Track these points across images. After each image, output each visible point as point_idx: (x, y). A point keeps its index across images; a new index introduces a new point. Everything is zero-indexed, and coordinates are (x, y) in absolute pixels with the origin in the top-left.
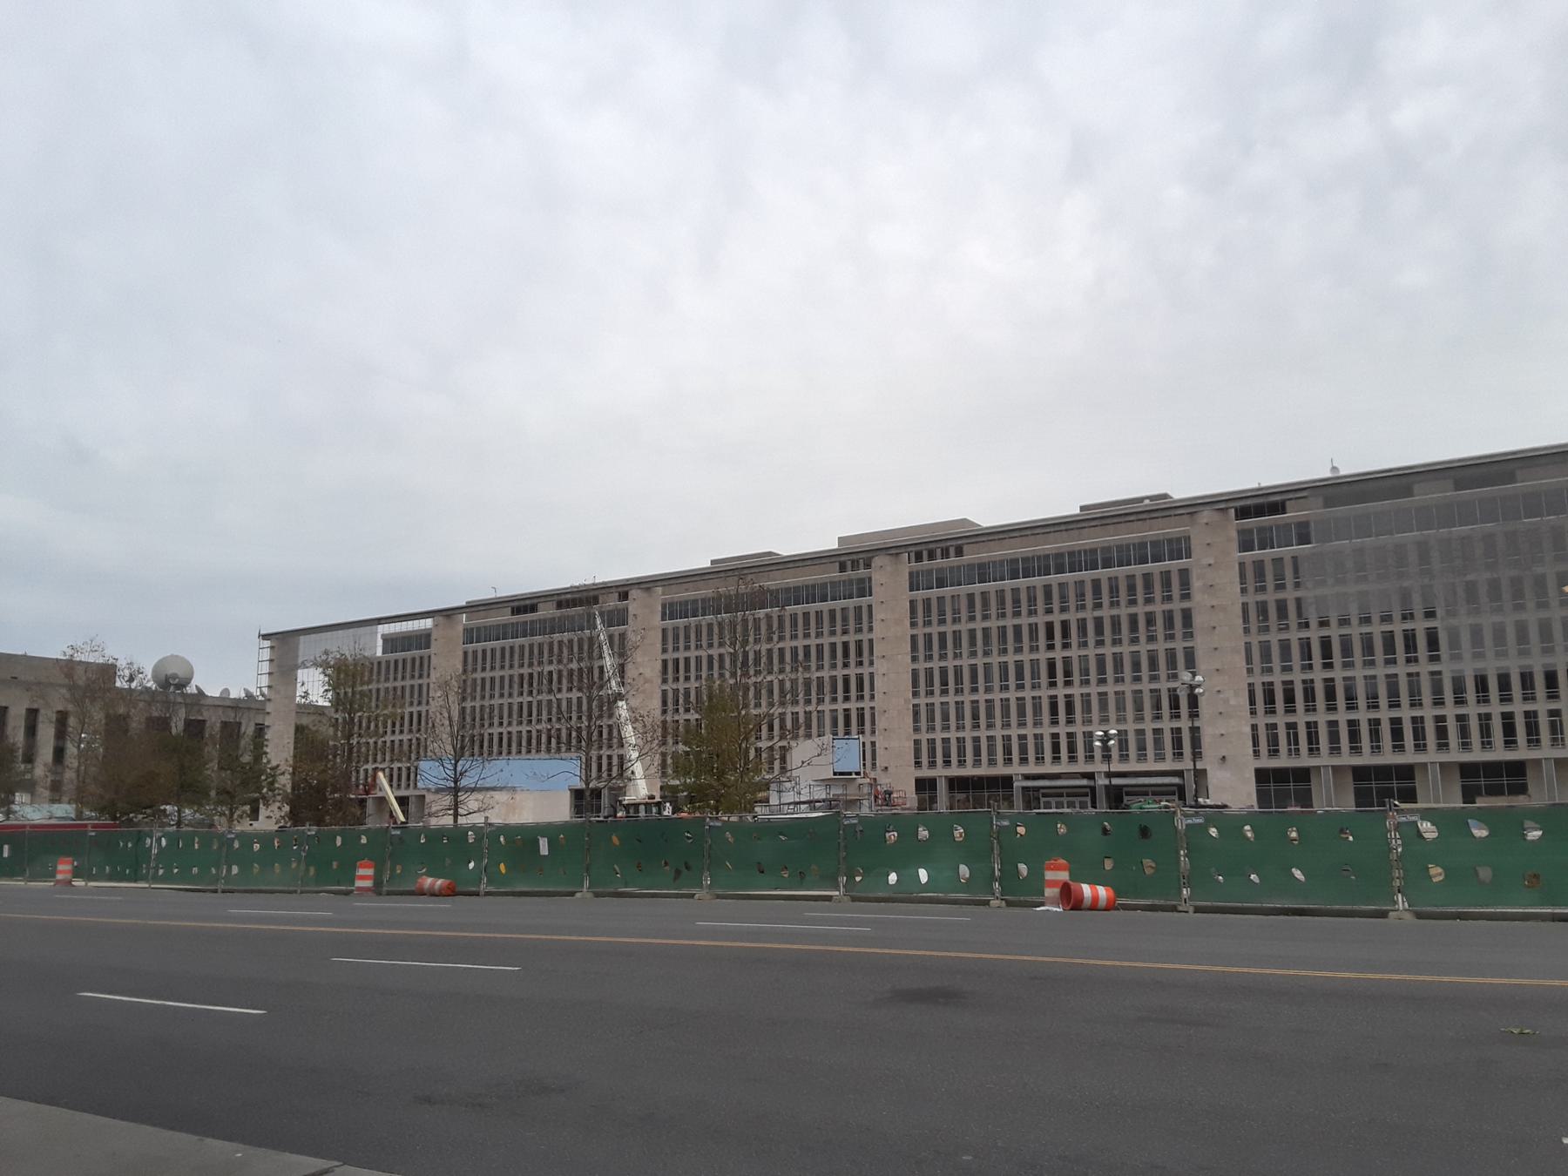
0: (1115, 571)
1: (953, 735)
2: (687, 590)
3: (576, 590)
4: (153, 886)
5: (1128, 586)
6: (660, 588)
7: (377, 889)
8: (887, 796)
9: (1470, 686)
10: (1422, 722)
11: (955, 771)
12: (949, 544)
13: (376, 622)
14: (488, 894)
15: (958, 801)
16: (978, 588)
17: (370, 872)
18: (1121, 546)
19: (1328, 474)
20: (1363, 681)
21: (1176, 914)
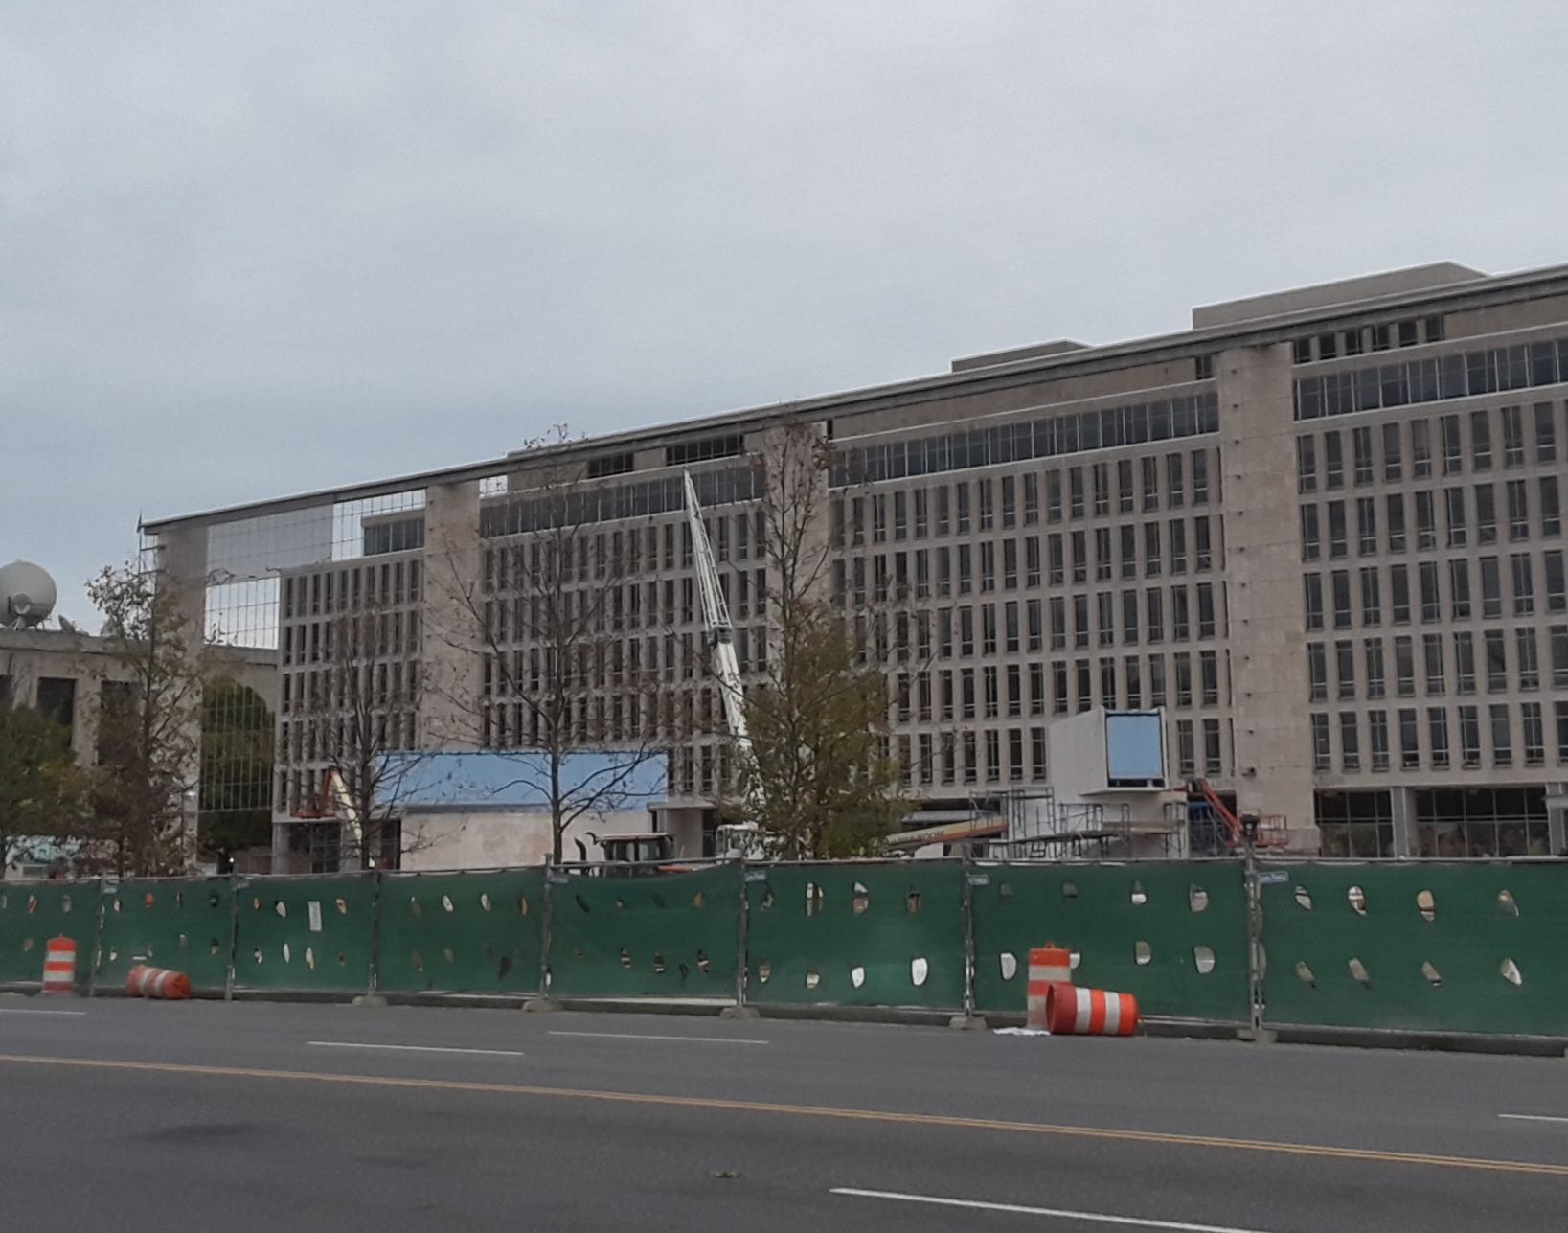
1: (1421, 704)
2: (905, 423)
3: (564, 449)
7: (82, 985)
8: (1249, 826)
10: (1538, 713)
11: (1428, 777)
12: (1386, 318)
13: (331, 497)
14: (236, 997)
15: (1440, 837)
16: (1466, 403)
17: (768, 973)
21: (1234, 1044)
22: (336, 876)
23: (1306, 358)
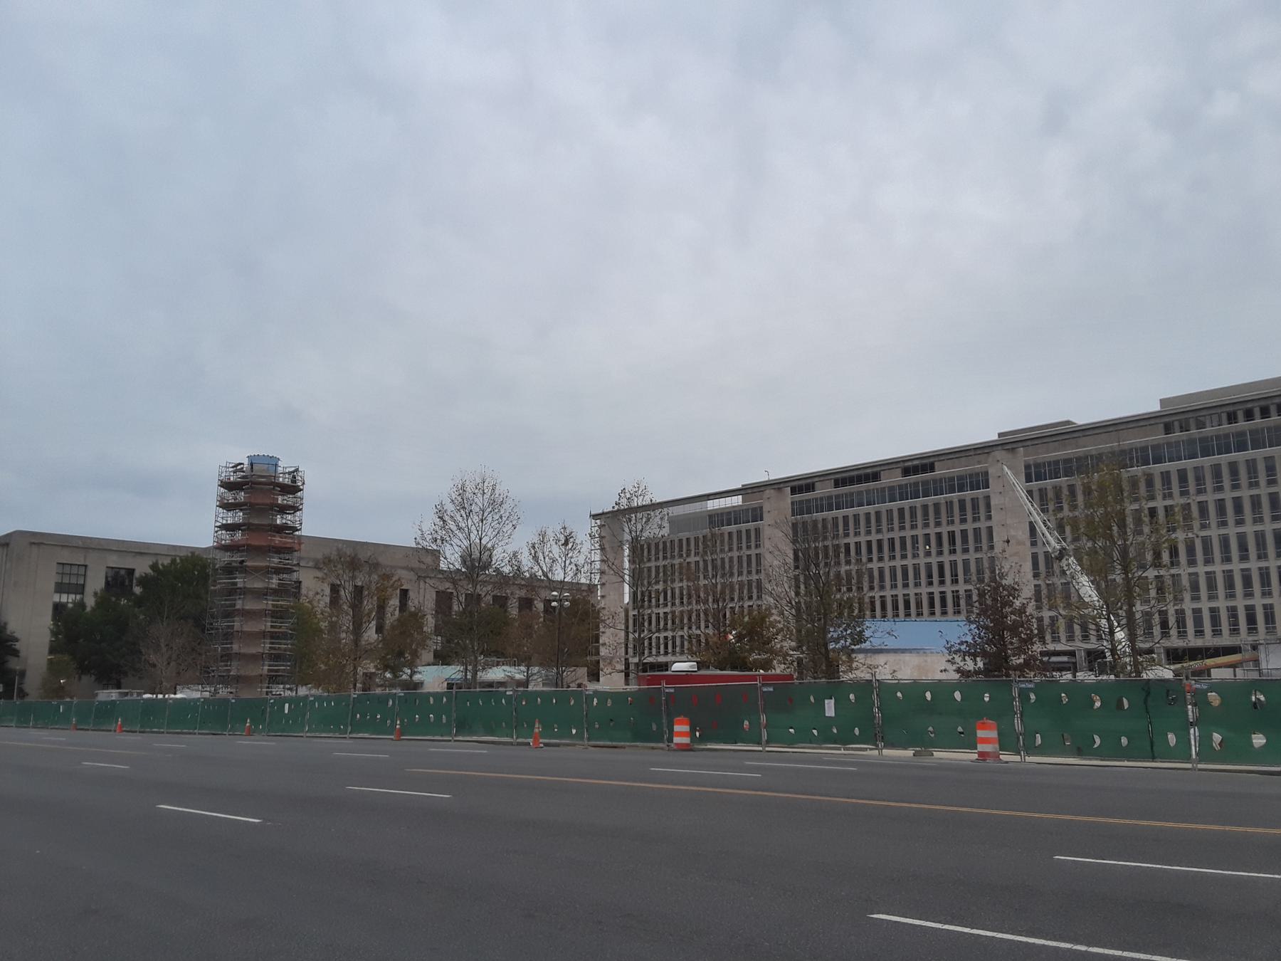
4: (767, 749)
6: (1022, 449)
12: (1269, 402)
13: (706, 498)
20: (1222, 574)
23: (1267, 416)
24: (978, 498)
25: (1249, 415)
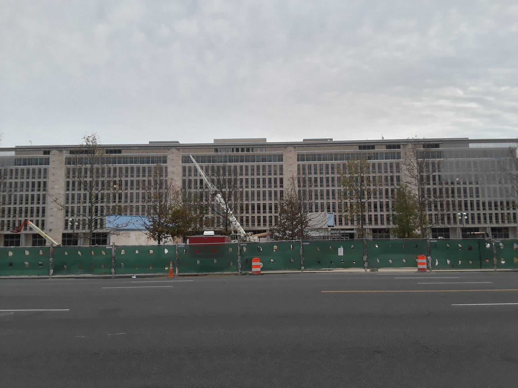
0: (322, 162)
4: (497, 270)
5: (331, 167)
9: (493, 205)
18: (324, 154)
19: (381, 139)
22: (507, 239)
24: (122, 168)
25: (243, 150)
